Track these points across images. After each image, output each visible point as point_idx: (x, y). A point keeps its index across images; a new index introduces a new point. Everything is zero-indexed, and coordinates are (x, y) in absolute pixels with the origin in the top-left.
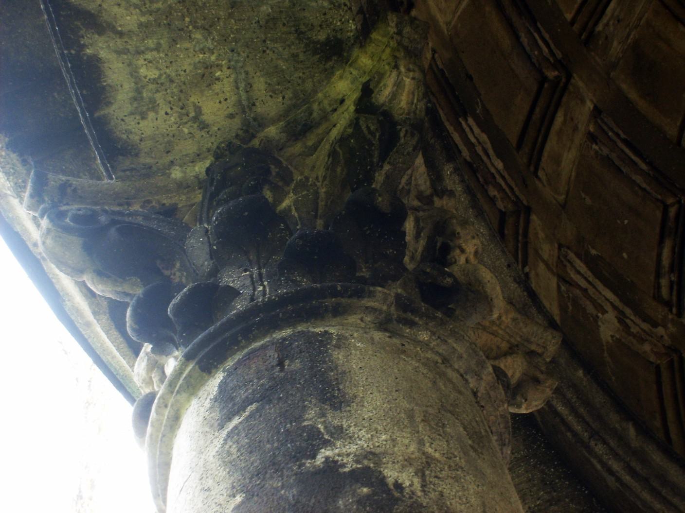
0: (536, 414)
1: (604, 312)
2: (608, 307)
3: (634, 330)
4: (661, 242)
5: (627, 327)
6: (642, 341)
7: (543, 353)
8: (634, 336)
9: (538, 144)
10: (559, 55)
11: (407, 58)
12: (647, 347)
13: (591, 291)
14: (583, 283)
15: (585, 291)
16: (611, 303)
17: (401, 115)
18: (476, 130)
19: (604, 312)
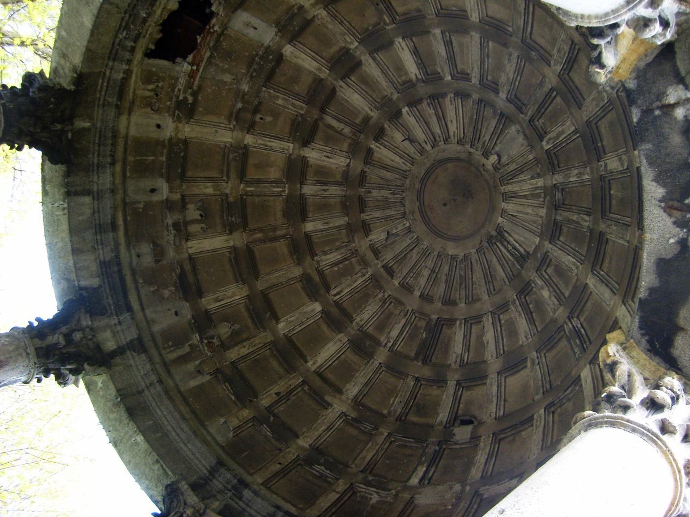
0: (306, 299)
1: (373, 495)
2: (373, 493)
3: (383, 495)
4: (432, 477)
5: (381, 496)
6: (387, 497)
7: (333, 484)
8: (383, 497)
9: (678, 479)
10: (373, 426)
11: (107, 422)
12: (389, 498)
13: (367, 491)
14: (364, 490)
15: (365, 492)
16: (375, 492)
17: (392, 442)
18: (319, 467)
19: (373, 495)
